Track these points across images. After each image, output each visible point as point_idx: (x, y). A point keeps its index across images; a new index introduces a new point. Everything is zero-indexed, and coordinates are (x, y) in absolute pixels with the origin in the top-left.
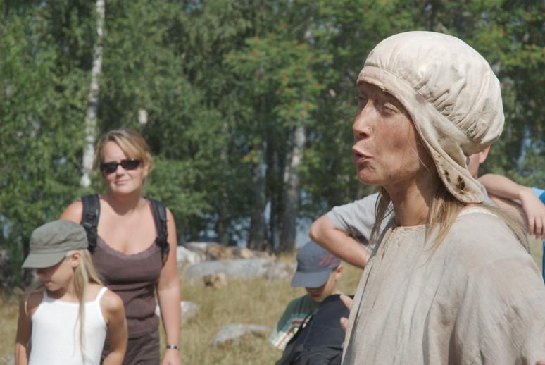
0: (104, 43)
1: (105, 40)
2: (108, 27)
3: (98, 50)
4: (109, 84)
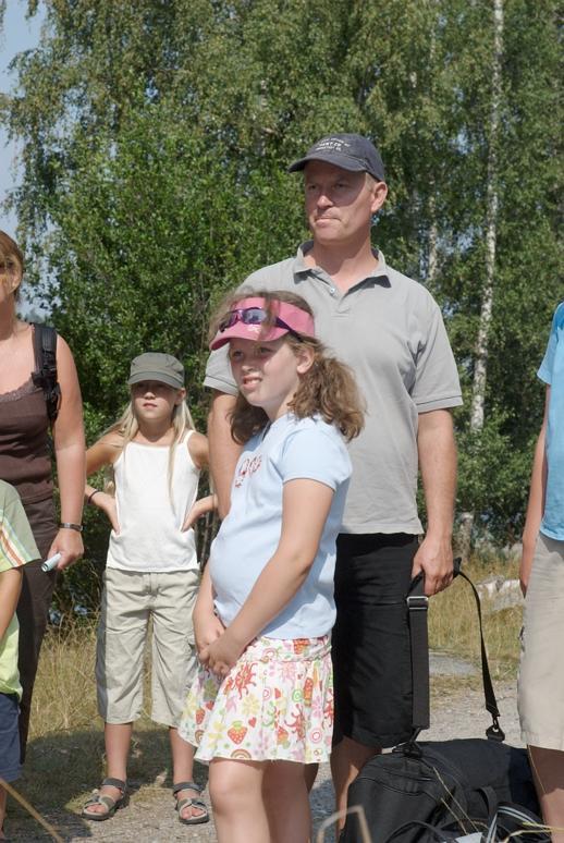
0: (496, 283)
1: (495, 278)
2: (499, 263)
3: (489, 291)
4: (498, 331)
